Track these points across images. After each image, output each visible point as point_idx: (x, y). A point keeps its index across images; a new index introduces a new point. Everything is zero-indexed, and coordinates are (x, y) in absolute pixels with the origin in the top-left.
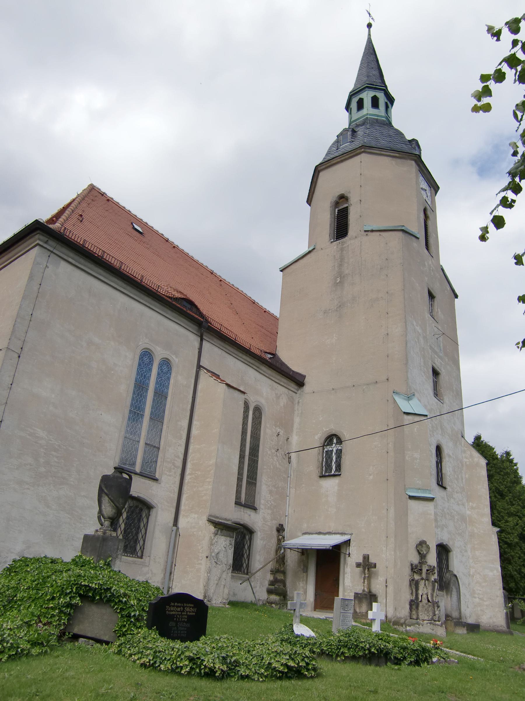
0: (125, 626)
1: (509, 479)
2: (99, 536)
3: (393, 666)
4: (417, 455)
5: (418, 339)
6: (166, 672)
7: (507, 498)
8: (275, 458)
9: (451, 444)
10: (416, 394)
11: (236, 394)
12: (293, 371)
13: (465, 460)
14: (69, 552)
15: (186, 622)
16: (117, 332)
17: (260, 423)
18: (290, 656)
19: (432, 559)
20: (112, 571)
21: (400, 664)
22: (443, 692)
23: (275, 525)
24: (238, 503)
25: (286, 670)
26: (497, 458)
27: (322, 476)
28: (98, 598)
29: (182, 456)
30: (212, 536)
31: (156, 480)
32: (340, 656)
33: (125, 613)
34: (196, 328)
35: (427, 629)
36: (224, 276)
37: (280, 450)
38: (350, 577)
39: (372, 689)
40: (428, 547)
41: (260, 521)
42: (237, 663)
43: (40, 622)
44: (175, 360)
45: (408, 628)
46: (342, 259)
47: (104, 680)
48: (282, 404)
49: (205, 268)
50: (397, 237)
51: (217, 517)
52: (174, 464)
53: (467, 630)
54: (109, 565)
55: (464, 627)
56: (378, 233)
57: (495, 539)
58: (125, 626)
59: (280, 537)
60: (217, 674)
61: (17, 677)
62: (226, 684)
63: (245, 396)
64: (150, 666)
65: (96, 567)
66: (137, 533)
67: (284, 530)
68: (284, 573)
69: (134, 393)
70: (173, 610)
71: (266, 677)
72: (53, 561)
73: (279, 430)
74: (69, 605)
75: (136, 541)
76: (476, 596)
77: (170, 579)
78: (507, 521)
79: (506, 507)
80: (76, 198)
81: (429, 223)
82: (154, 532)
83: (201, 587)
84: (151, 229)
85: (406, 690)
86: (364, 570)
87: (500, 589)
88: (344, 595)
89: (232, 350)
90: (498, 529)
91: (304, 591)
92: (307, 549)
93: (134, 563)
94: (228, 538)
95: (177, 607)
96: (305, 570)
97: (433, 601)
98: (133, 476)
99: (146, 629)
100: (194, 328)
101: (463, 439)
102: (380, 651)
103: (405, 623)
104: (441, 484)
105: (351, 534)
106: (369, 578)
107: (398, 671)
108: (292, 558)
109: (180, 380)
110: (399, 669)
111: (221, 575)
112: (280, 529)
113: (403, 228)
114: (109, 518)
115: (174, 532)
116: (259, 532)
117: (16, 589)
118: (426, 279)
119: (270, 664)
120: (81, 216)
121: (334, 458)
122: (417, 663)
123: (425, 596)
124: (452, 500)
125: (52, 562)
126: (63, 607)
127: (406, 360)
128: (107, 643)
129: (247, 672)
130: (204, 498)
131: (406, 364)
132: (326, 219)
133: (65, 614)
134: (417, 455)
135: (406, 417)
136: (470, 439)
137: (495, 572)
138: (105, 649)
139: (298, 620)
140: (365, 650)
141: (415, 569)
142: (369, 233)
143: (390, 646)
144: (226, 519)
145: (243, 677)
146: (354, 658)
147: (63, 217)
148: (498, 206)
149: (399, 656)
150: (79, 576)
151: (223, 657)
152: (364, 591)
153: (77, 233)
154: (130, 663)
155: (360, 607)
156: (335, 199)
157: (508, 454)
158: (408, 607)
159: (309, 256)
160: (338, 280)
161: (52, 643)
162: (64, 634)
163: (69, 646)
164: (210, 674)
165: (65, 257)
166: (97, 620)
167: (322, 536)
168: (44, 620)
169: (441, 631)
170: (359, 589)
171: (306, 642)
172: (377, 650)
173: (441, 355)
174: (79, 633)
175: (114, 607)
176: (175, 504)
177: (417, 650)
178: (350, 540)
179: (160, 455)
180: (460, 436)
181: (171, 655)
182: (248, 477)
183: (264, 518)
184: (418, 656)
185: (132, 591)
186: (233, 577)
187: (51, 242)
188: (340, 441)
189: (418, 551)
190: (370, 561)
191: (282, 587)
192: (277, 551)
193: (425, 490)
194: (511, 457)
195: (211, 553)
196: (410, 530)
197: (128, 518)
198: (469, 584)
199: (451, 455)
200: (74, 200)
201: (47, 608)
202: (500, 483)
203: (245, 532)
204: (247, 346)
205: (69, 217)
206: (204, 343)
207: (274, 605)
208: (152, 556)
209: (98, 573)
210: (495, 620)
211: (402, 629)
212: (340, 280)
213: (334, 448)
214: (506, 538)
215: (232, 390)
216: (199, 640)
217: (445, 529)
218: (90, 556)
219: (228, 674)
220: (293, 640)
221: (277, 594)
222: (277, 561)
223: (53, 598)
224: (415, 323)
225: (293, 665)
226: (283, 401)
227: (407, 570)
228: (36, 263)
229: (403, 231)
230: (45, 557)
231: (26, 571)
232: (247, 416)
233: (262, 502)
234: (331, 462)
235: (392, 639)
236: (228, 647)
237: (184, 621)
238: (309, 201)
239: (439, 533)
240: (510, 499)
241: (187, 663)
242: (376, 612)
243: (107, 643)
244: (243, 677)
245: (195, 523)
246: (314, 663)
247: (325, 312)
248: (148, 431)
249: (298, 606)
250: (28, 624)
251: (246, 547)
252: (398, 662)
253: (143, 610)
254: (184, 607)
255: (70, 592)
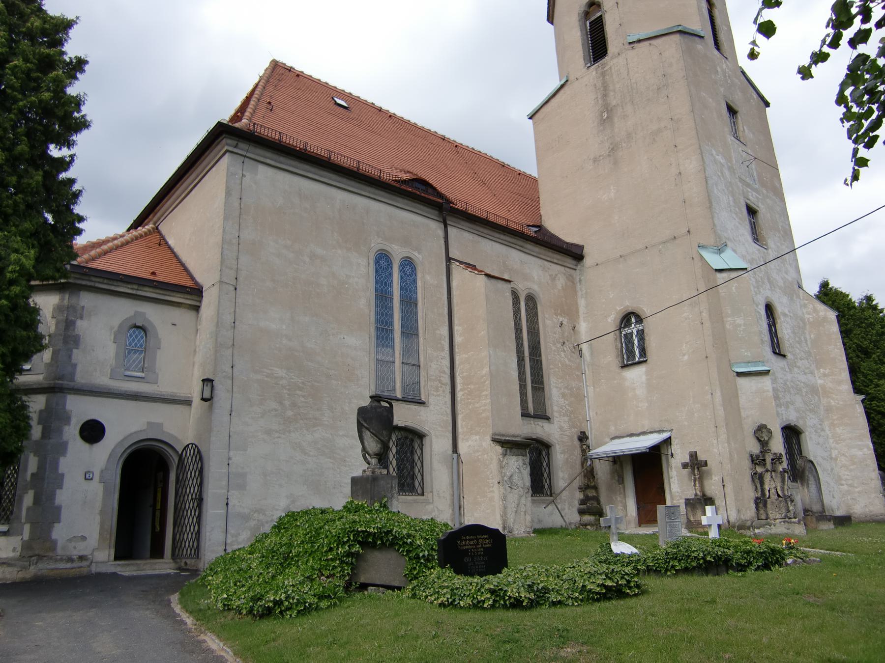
0: (415, 568)
1: (874, 332)
2: (368, 477)
3: (735, 574)
4: (739, 321)
5: (722, 173)
6: (469, 608)
7: (874, 356)
8: (563, 354)
9: (785, 300)
10: (729, 243)
11: (500, 285)
12: (567, 243)
13: (807, 316)
14: (339, 498)
15: (483, 556)
16: (342, 241)
17: (536, 314)
18: (606, 576)
19: (778, 445)
20: (390, 512)
21: (745, 571)
22: (798, 594)
23: (575, 432)
24: (525, 415)
25: (604, 591)
26: (854, 307)
27: (624, 366)
28: (379, 542)
29: (448, 371)
30: (500, 457)
31: (422, 403)
32: (670, 571)
33: (412, 555)
34: (437, 212)
35: (779, 529)
36: (459, 140)
37: (567, 343)
38: (676, 481)
39: (709, 599)
40: (770, 432)
41: (557, 431)
42: (546, 590)
43: (322, 575)
44: (417, 257)
45: (757, 531)
46: (605, 87)
47: (402, 623)
48: (559, 287)
49: (435, 134)
50: (672, 46)
51: (503, 435)
52: (440, 381)
53: (834, 524)
54: (385, 506)
55: (830, 521)
56: (647, 43)
57: (860, 410)
58: (415, 568)
59: (584, 447)
60: (524, 604)
61: (311, 629)
62: (535, 612)
63: (512, 285)
64: (449, 604)
65: (371, 511)
66: (413, 468)
67: (587, 438)
68: (595, 488)
69: (377, 306)
70: (466, 544)
71: (582, 600)
72: (323, 512)
73: (561, 319)
74: (349, 554)
75: (413, 477)
76: (843, 482)
77: (460, 514)
78: (877, 386)
79: (874, 367)
80: (259, 82)
81: (716, 13)
82: (431, 463)
83: (498, 517)
84: (357, 100)
85: (750, 596)
86: (693, 470)
87: (874, 470)
88: (672, 502)
89: (486, 231)
90: (863, 397)
91: (624, 507)
92: (619, 457)
93: (415, 501)
94: (521, 457)
95: (470, 540)
96: (621, 480)
97: (784, 495)
98: (394, 403)
99: (438, 569)
100: (434, 213)
101: (801, 291)
102: (718, 558)
103: (752, 526)
104: (777, 350)
105: (671, 430)
106: (701, 479)
107: (742, 579)
108: (602, 471)
109: (429, 280)
110: (742, 576)
111: (519, 500)
112: (583, 438)
113: (680, 28)
114: (376, 455)
115: (455, 459)
116: (558, 447)
117: (290, 545)
118: (722, 89)
119: (584, 586)
120: (270, 103)
121: (636, 342)
122: (766, 566)
123: (773, 491)
124: (796, 370)
125: (322, 513)
126: (343, 556)
127: (710, 203)
128: (399, 588)
129: (559, 598)
130: (484, 415)
131: (710, 207)
132: (576, 37)
133: (347, 563)
134: (739, 321)
135: (719, 275)
136: (813, 288)
137: (865, 450)
138: (398, 596)
139: (615, 537)
140: (699, 560)
141: (757, 460)
142: (636, 45)
143: (729, 552)
144: (514, 436)
145: (554, 604)
146: (686, 570)
147: (249, 110)
148: (761, 10)
149: (743, 562)
150: (354, 522)
151: (529, 585)
152: (696, 495)
153: (272, 126)
154: (428, 605)
155: (694, 515)
156: (583, 9)
157: (869, 299)
158: (753, 506)
159: (562, 92)
160: (605, 115)
161: (340, 594)
162: (351, 584)
163: (358, 596)
164: (517, 604)
165: (262, 159)
166: (382, 566)
167: (635, 438)
168: (327, 573)
169: (799, 530)
170: (690, 494)
171: (629, 560)
172: (714, 558)
173: (756, 186)
174: (366, 582)
175: (398, 550)
176: (450, 428)
177: (764, 552)
178: (670, 438)
179: (422, 373)
180: (796, 287)
181: (470, 590)
182: (532, 383)
183: (561, 428)
184: (766, 558)
185: (416, 530)
186: (533, 502)
187: (241, 145)
188: (640, 320)
189: (757, 438)
190: (699, 458)
191: (595, 504)
192: (582, 464)
193: (755, 363)
194: (874, 303)
195: (503, 477)
196: (743, 414)
197: (398, 452)
198: (832, 469)
199: (787, 312)
200: (257, 85)
201: (327, 560)
202: (862, 337)
203: (541, 447)
204: (503, 222)
205: (257, 105)
206: (449, 228)
207: (589, 527)
208: (434, 490)
209: (375, 517)
210: (871, 508)
211: (749, 533)
212: (607, 115)
213: (634, 329)
214: (878, 406)
215: (493, 281)
216: (501, 573)
217: (791, 407)
218: (363, 500)
219: (538, 602)
220: (612, 559)
221: (590, 514)
222: (585, 476)
223: (331, 549)
224: (714, 152)
225: (610, 584)
226: (561, 282)
227: (747, 463)
228: (230, 175)
229: (680, 32)
230: (314, 508)
231: (296, 525)
232: (519, 309)
233: (555, 408)
234: (633, 347)
235: (732, 544)
236: (534, 575)
237: (480, 555)
238: (550, 19)
239: (783, 412)
240: (878, 356)
241: (488, 596)
242: (709, 516)
243: (399, 588)
244: (554, 604)
245: (477, 445)
246: (636, 579)
247: (595, 160)
248: (403, 348)
249: (613, 521)
250: (310, 579)
251: (545, 464)
252: (742, 568)
253: (432, 549)
254: (477, 540)
255: (348, 541)
